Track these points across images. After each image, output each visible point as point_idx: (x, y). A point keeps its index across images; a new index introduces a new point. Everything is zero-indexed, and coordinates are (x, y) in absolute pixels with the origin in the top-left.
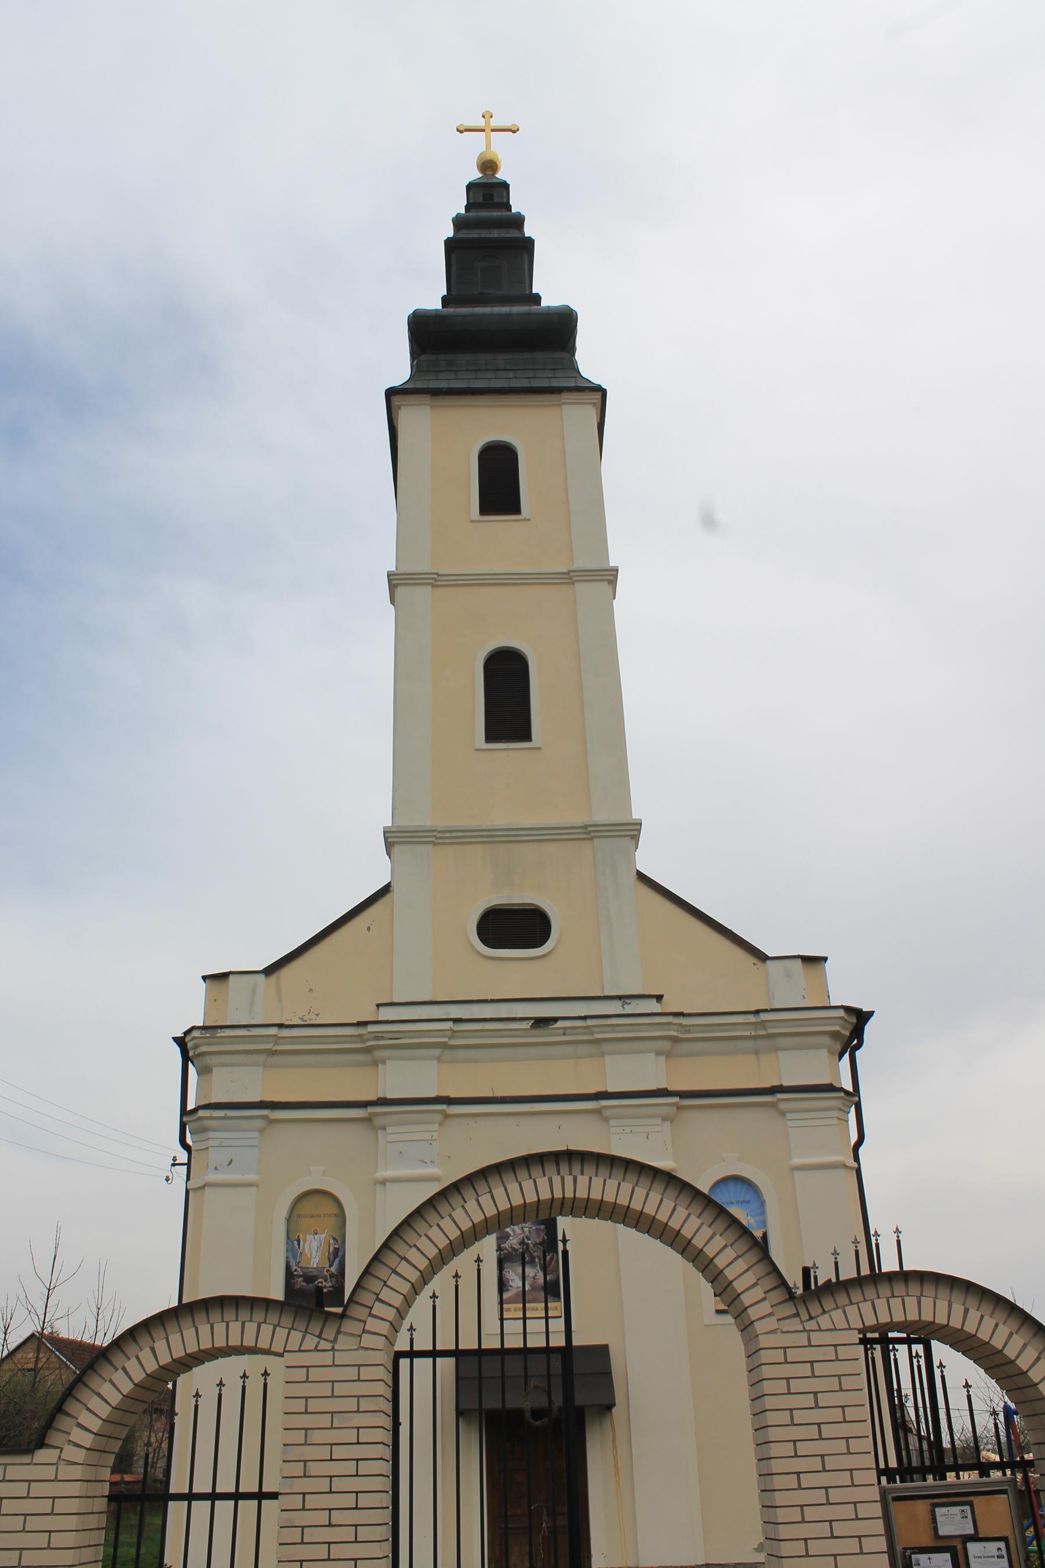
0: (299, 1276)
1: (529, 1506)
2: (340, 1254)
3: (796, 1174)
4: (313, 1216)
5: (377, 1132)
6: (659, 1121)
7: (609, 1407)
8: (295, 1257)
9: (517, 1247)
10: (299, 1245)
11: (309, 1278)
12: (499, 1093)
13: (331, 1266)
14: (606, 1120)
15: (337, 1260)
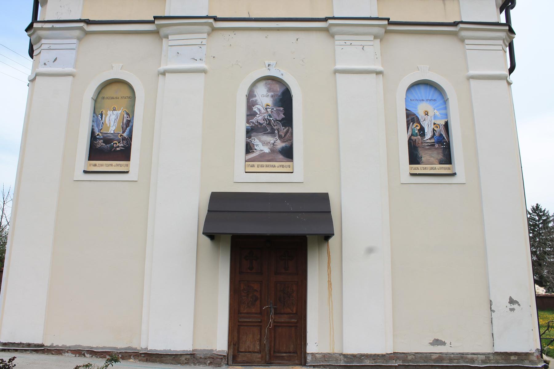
0: (100, 139)
1: (261, 307)
2: (131, 124)
3: (472, 82)
4: (113, 98)
5: (162, 39)
6: (372, 38)
7: (327, 237)
8: (98, 126)
9: (262, 122)
10: (102, 118)
11: (107, 141)
12: (253, 16)
13: (123, 132)
14: (332, 36)
15: (128, 129)
